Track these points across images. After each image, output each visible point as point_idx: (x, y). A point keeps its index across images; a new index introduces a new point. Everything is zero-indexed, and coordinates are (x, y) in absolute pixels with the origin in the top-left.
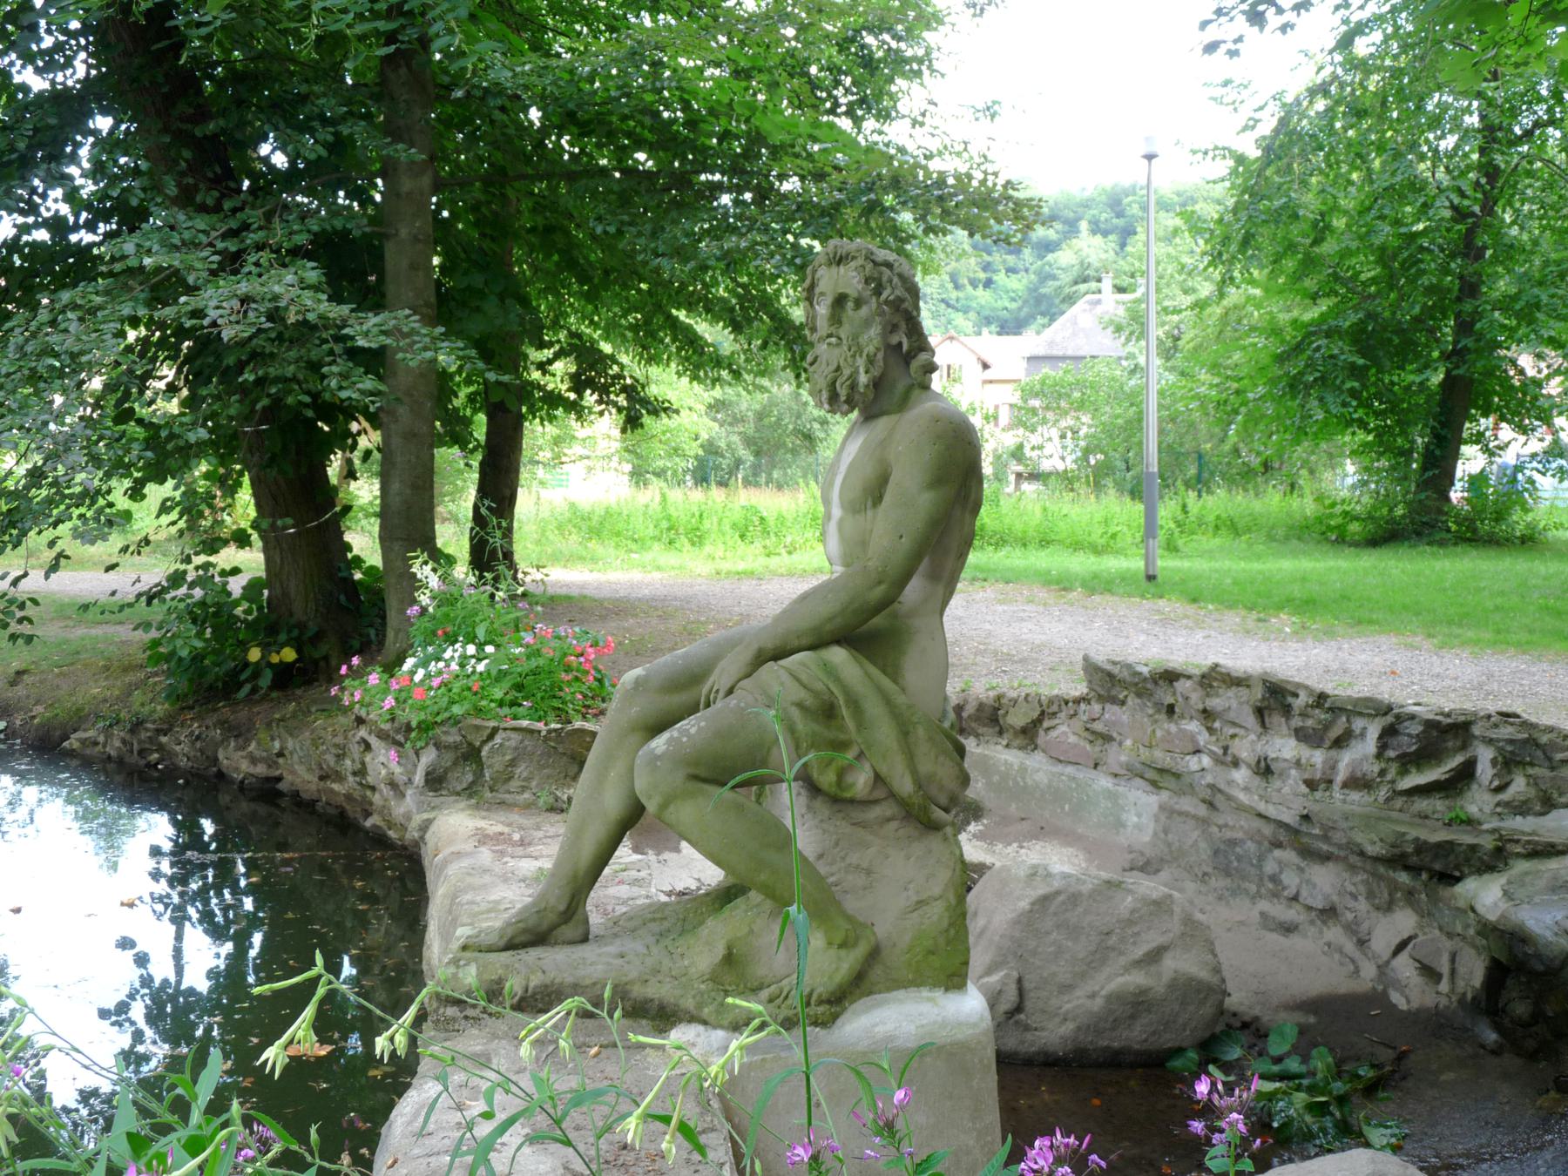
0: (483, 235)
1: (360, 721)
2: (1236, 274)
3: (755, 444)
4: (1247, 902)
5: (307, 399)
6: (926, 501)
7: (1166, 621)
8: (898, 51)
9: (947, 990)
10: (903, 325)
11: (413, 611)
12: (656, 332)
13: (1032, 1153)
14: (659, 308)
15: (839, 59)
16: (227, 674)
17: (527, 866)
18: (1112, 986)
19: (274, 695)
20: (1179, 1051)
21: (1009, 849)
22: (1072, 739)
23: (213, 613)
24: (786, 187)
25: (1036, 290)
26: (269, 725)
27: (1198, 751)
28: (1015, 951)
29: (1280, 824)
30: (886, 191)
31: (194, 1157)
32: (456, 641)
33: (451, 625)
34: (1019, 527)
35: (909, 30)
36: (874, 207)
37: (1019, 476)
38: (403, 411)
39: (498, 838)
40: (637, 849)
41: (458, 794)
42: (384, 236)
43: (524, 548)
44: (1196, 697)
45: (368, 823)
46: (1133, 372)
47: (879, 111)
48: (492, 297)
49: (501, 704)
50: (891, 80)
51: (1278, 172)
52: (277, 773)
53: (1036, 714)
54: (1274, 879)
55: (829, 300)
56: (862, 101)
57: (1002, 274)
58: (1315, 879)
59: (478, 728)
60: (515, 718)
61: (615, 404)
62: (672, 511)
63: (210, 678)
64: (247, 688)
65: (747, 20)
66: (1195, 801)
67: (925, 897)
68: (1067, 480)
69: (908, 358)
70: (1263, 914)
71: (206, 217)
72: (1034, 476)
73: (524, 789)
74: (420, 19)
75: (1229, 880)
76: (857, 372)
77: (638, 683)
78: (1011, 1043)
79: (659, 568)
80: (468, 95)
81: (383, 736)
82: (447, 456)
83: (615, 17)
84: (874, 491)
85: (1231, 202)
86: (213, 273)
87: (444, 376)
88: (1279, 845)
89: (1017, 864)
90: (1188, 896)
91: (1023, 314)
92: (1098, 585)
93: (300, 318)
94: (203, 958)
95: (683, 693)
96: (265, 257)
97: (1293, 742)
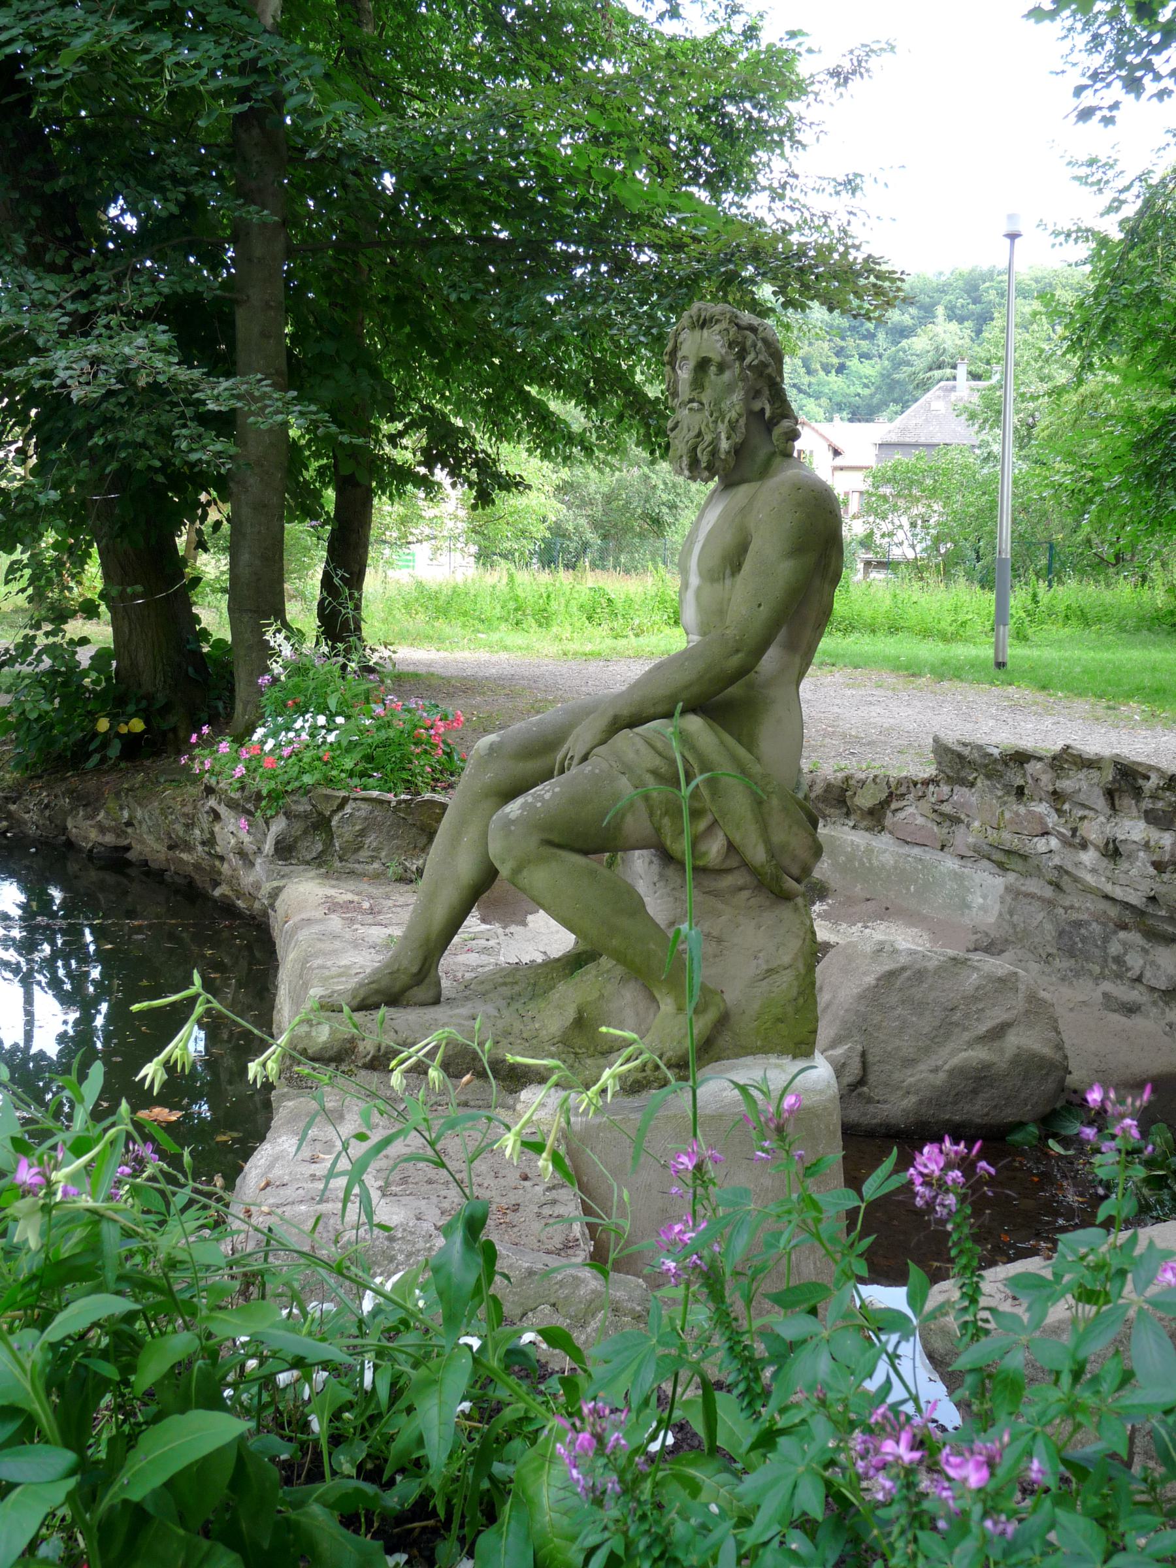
0: (333, 304)
1: (210, 790)
2: (1095, 360)
3: (603, 527)
4: (1090, 983)
5: (158, 464)
6: (785, 570)
7: (1015, 708)
8: (759, 121)
9: (794, 1057)
10: (766, 392)
11: (265, 680)
12: (506, 407)
13: (920, 1160)
14: (510, 382)
15: (699, 129)
16: (75, 744)
17: (377, 934)
18: (955, 1061)
19: (123, 765)
20: (1020, 1125)
21: (854, 929)
22: (920, 821)
23: (63, 680)
24: (643, 258)
25: (889, 376)
26: (117, 795)
27: (1047, 833)
28: (860, 1025)
29: (1127, 905)
30: (744, 261)
31: (78, 1157)
32: (307, 712)
33: (302, 696)
34: (868, 613)
35: (771, 98)
36: (731, 278)
37: (868, 564)
38: (253, 481)
39: (347, 906)
40: (484, 920)
41: (308, 863)
42: (234, 302)
43: (372, 627)
44: (1046, 779)
45: (217, 893)
46: (986, 460)
47: (739, 183)
48: (345, 366)
49: (351, 774)
50: (752, 151)
51: (1141, 256)
52: (126, 842)
53: (884, 796)
54: (1118, 960)
55: (692, 364)
56: (722, 173)
57: (855, 360)
58: (1160, 961)
59: (328, 798)
60: (365, 789)
61: (466, 479)
62: (519, 592)
63: (59, 747)
64: (96, 758)
65: (607, 83)
66: (1042, 882)
67: (773, 965)
68: (918, 569)
69: (770, 425)
70: (1106, 995)
71: (56, 277)
72: (883, 565)
73: (373, 859)
74: (274, 77)
75: (1073, 961)
76: (718, 437)
77: (492, 748)
78: (854, 1116)
79: (506, 648)
80: (322, 157)
81: (232, 805)
82: (298, 532)
83: (471, 80)
84: (732, 559)
85: (1091, 286)
86: (63, 335)
87: (294, 447)
88: (1124, 927)
89: (860, 943)
90: (1030, 974)
91: (875, 401)
92: (947, 672)
93: (151, 380)
94: (53, 1022)
95: (538, 757)
96: (114, 319)
97: (1142, 824)
